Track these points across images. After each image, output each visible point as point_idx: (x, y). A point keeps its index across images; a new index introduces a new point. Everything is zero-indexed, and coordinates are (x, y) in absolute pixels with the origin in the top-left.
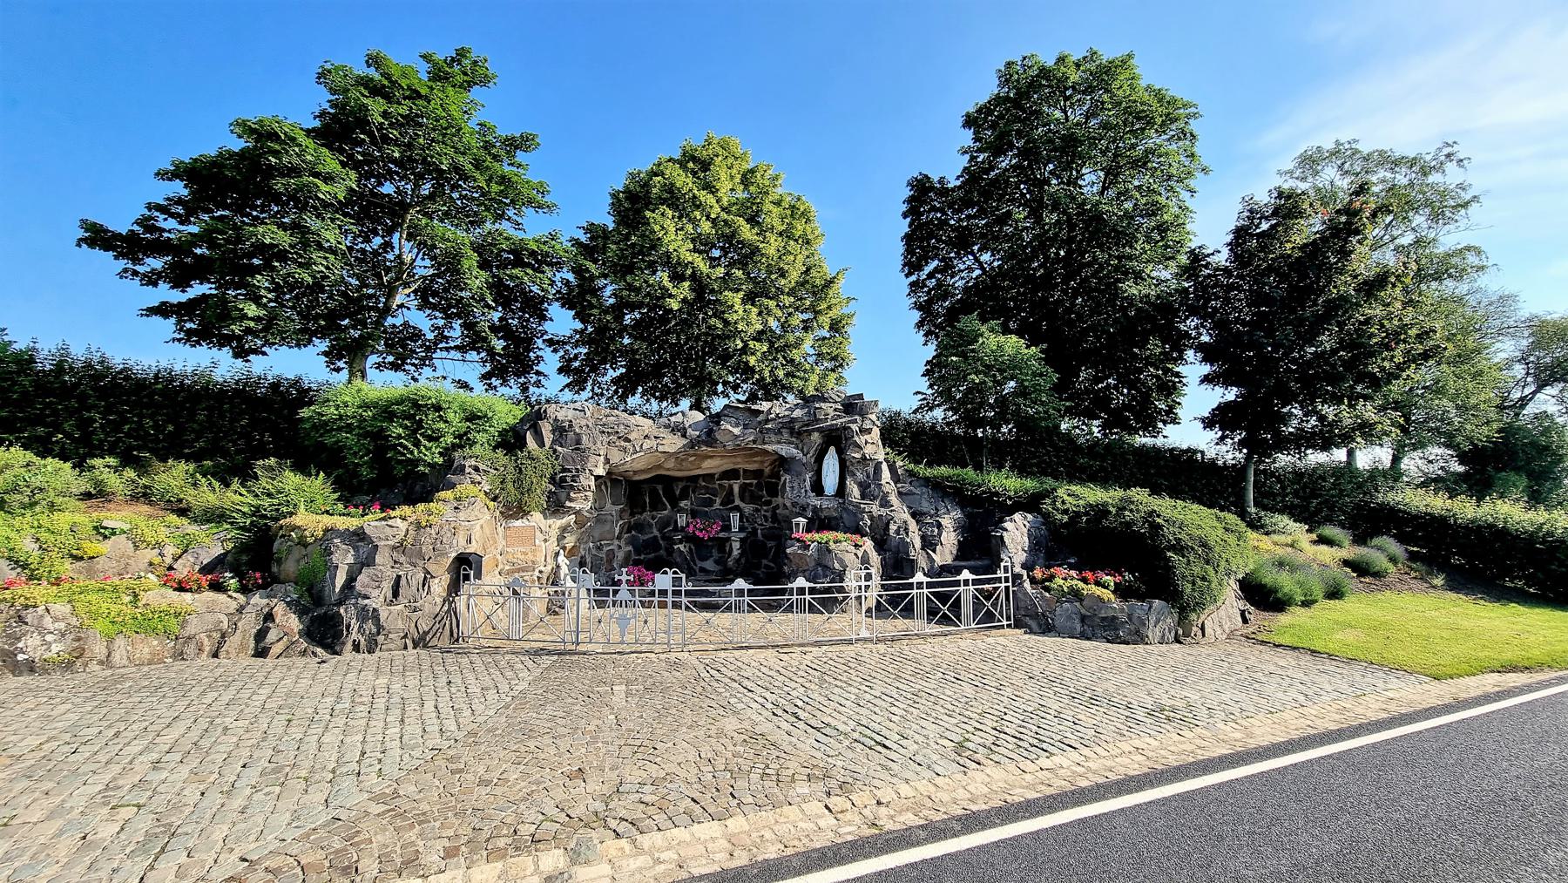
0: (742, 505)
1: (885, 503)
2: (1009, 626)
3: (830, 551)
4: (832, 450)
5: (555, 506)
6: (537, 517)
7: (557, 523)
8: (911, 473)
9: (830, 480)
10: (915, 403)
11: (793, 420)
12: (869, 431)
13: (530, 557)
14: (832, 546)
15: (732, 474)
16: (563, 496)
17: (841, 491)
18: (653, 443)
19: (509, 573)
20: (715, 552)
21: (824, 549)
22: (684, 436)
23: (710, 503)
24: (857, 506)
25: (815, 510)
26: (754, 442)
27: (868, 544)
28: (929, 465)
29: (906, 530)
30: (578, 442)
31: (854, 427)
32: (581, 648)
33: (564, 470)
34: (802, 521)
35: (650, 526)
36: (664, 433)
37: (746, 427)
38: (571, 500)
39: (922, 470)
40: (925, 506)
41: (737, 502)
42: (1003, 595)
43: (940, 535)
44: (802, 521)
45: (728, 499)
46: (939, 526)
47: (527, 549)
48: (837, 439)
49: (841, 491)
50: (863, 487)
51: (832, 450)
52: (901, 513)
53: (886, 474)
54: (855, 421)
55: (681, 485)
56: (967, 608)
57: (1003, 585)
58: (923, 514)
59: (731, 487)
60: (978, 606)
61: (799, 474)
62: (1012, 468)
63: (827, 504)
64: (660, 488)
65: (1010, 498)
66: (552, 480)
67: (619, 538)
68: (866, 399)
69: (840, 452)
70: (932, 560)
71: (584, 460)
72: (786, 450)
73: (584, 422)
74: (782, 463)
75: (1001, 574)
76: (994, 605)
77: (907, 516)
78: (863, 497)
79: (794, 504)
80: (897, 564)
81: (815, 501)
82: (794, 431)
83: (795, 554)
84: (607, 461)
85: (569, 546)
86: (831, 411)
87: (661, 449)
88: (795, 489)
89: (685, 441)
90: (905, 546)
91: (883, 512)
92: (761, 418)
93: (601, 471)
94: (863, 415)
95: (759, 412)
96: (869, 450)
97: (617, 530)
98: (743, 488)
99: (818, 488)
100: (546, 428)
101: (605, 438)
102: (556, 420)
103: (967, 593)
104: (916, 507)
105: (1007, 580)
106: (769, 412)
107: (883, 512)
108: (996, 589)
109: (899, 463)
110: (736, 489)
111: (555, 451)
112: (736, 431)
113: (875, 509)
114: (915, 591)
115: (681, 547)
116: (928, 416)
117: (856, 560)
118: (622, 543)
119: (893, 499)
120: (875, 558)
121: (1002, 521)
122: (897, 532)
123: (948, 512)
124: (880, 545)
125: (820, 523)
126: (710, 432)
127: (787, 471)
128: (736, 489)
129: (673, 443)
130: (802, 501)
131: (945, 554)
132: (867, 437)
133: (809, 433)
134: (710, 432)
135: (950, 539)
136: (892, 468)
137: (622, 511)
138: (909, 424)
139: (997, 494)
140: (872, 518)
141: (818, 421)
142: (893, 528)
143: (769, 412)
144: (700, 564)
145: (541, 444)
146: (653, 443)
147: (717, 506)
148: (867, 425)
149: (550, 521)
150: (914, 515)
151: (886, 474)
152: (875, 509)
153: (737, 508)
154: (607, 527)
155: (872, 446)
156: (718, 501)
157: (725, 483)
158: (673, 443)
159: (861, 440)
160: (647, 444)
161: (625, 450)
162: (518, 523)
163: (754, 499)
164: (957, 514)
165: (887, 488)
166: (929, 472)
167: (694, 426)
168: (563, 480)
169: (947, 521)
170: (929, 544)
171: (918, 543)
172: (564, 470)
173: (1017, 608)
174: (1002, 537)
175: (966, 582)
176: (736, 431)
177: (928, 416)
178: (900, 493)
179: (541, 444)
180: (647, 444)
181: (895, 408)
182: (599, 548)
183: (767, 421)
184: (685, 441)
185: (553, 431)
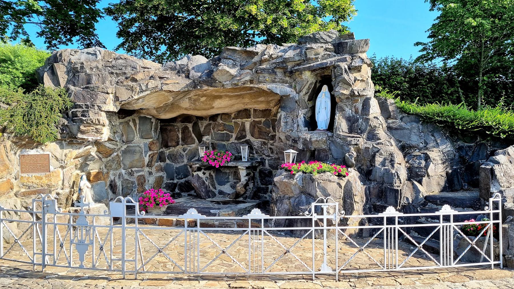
0: (252, 139)
1: (372, 136)
2: (497, 266)
3: (313, 180)
4: (325, 88)
5: (69, 138)
6: (52, 148)
7: (73, 153)
8: (402, 110)
9: (322, 117)
10: (416, 53)
11: (285, 61)
12: (358, 69)
13: (45, 181)
14: (316, 175)
15: (245, 113)
16: (74, 128)
17: (331, 127)
18: (157, 83)
19: (24, 195)
20: (231, 178)
21: (308, 179)
22: (188, 77)
23: (228, 137)
24: (344, 139)
25: (305, 142)
26: (251, 82)
27: (353, 174)
28: (421, 103)
29: (392, 162)
30: (89, 82)
31: (344, 65)
32: (48, 270)
33: (76, 106)
34: (292, 152)
35: (182, 157)
36: (168, 74)
37: (242, 67)
38: (83, 132)
39: (414, 107)
40: (414, 140)
41: (249, 137)
42: (491, 232)
43: (427, 167)
44: (292, 152)
45: (241, 136)
46: (427, 158)
47: (43, 175)
48: (326, 78)
49: (331, 127)
50: (352, 122)
51: (325, 88)
52: (389, 146)
53: (375, 108)
54: (345, 60)
55: (206, 123)
56: (447, 244)
57: (492, 222)
58: (411, 147)
59: (243, 124)
60: (459, 245)
61: (293, 110)
62: (507, 104)
63: (314, 137)
64: (190, 126)
65: (504, 132)
66: (65, 112)
67: (149, 165)
68: (357, 37)
69: (331, 89)
70: (417, 191)
71: (93, 97)
72: (281, 89)
73: (94, 64)
74: (282, 101)
75: (489, 210)
76: (480, 243)
77: (394, 149)
78: (351, 130)
79: (288, 138)
80: (382, 193)
81: (306, 135)
82: (289, 71)
83: (281, 182)
84: (117, 99)
85: (94, 172)
86: (322, 52)
87: (165, 88)
88: (291, 124)
89: (188, 82)
90: (390, 176)
91: (370, 144)
92: (256, 59)
93: (112, 107)
94: (353, 54)
95: (253, 54)
96: (358, 87)
97: (147, 159)
98: (254, 125)
99: (311, 124)
100: (61, 70)
101: (114, 79)
102: (70, 62)
103: (448, 230)
104: (405, 141)
105: (496, 217)
106: (263, 54)
107: (370, 144)
108: (484, 226)
109: (391, 100)
110: (248, 126)
111: (68, 90)
112: (233, 71)
113: (362, 142)
114: (385, 227)
115: (200, 174)
116: (427, 65)
117: (336, 186)
118: (154, 170)
119: (382, 133)
120: (359, 188)
121: (493, 153)
122: (383, 164)
123: (438, 145)
124: (366, 175)
125: (312, 155)
126: (210, 73)
127: (283, 108)
128: (248, 126)
129: (177, 83)
130: (294, 135)
131: (432, 184)
132: (357, 75)
133: (301, 72)
134: (210, 73)
135: (437, 172)
136: (383, 106)
137: (152, 143)
138: (408, 72)
139: (490, 128)
140: (358, 150)
141: (307, 60)
142: (379, 160)
143: (263, 54)
144: (219, 188)
145: (57, 83)
146: (157, 83)
147: (233, 140)
148: (356, 63)
149: (66, 151)
150: (402, 148)
151: (375, 108)
152: (362, 142)
153: (248, 142)
154: (137, 157)
155: (363, 83)
156: (234, 136)
157: (239, 121)
158: (177, 83)
159: (351, 77)
160: (152, 84)
161: (132, 89)
162: (33, 152)
163: (261, 134)
164: (447, 147)
165: (374, 123)
166: (420, 109)
167: (198, 68)
168: (74, 115)
169: (435, 154)
170: (415, 175)
171: (403, 174)
172: (76, 106)
173: (507, 247)
174: (492, 171)
175: (447, 218)
176: (233, 71)
177: (427, 65)
178: (389, 128)
179: (57, 83)
180: (152, 84)
181: (397, 57)
182: (131, 174)
183: (261, 62)
184: (188, 82)
185: (68, 72)
